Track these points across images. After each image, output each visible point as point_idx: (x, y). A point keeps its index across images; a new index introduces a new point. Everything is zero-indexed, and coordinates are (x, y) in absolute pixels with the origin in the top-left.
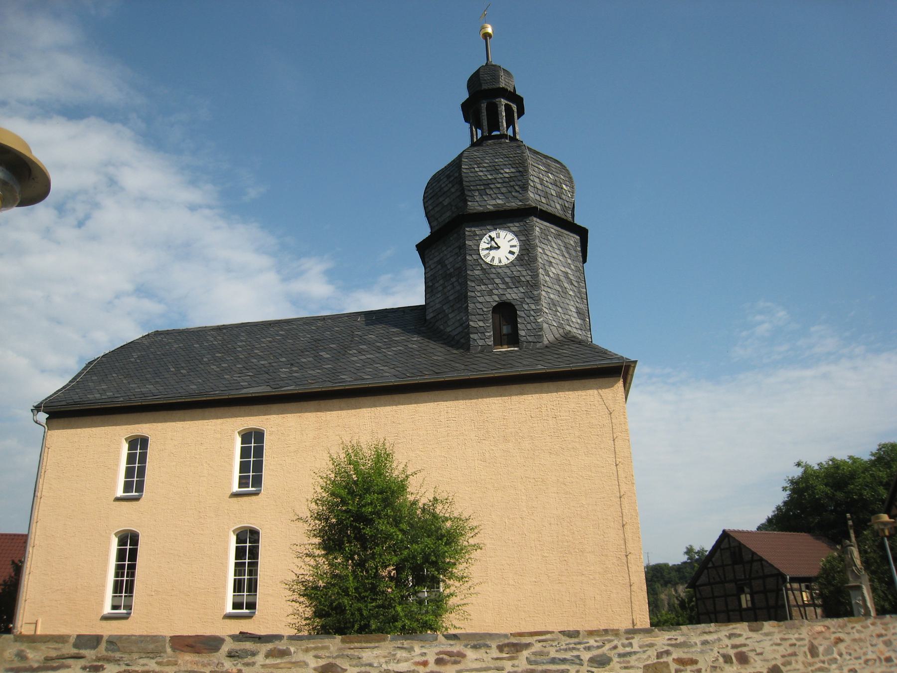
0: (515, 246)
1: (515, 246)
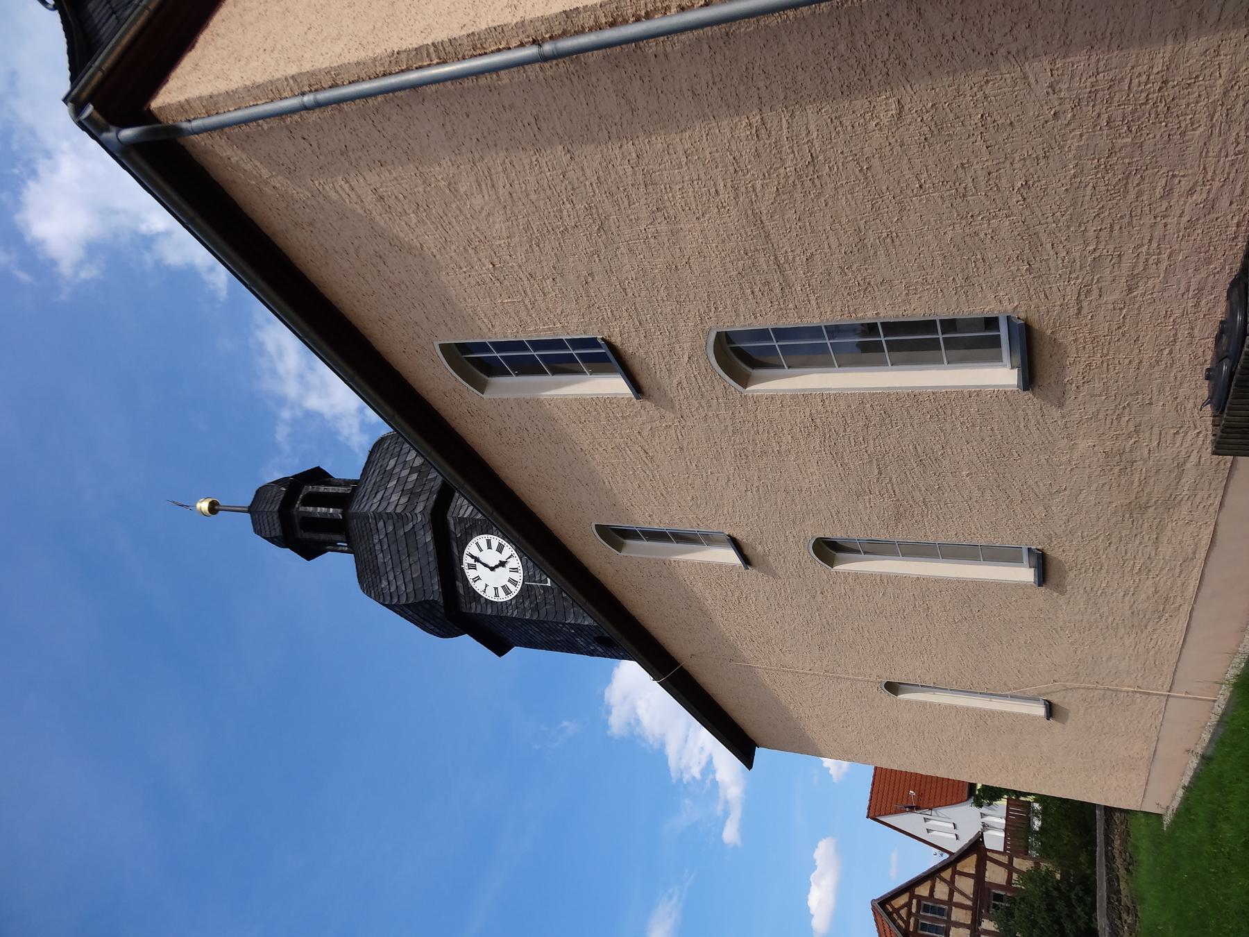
0: (489, 542)
1: (489, 542)
